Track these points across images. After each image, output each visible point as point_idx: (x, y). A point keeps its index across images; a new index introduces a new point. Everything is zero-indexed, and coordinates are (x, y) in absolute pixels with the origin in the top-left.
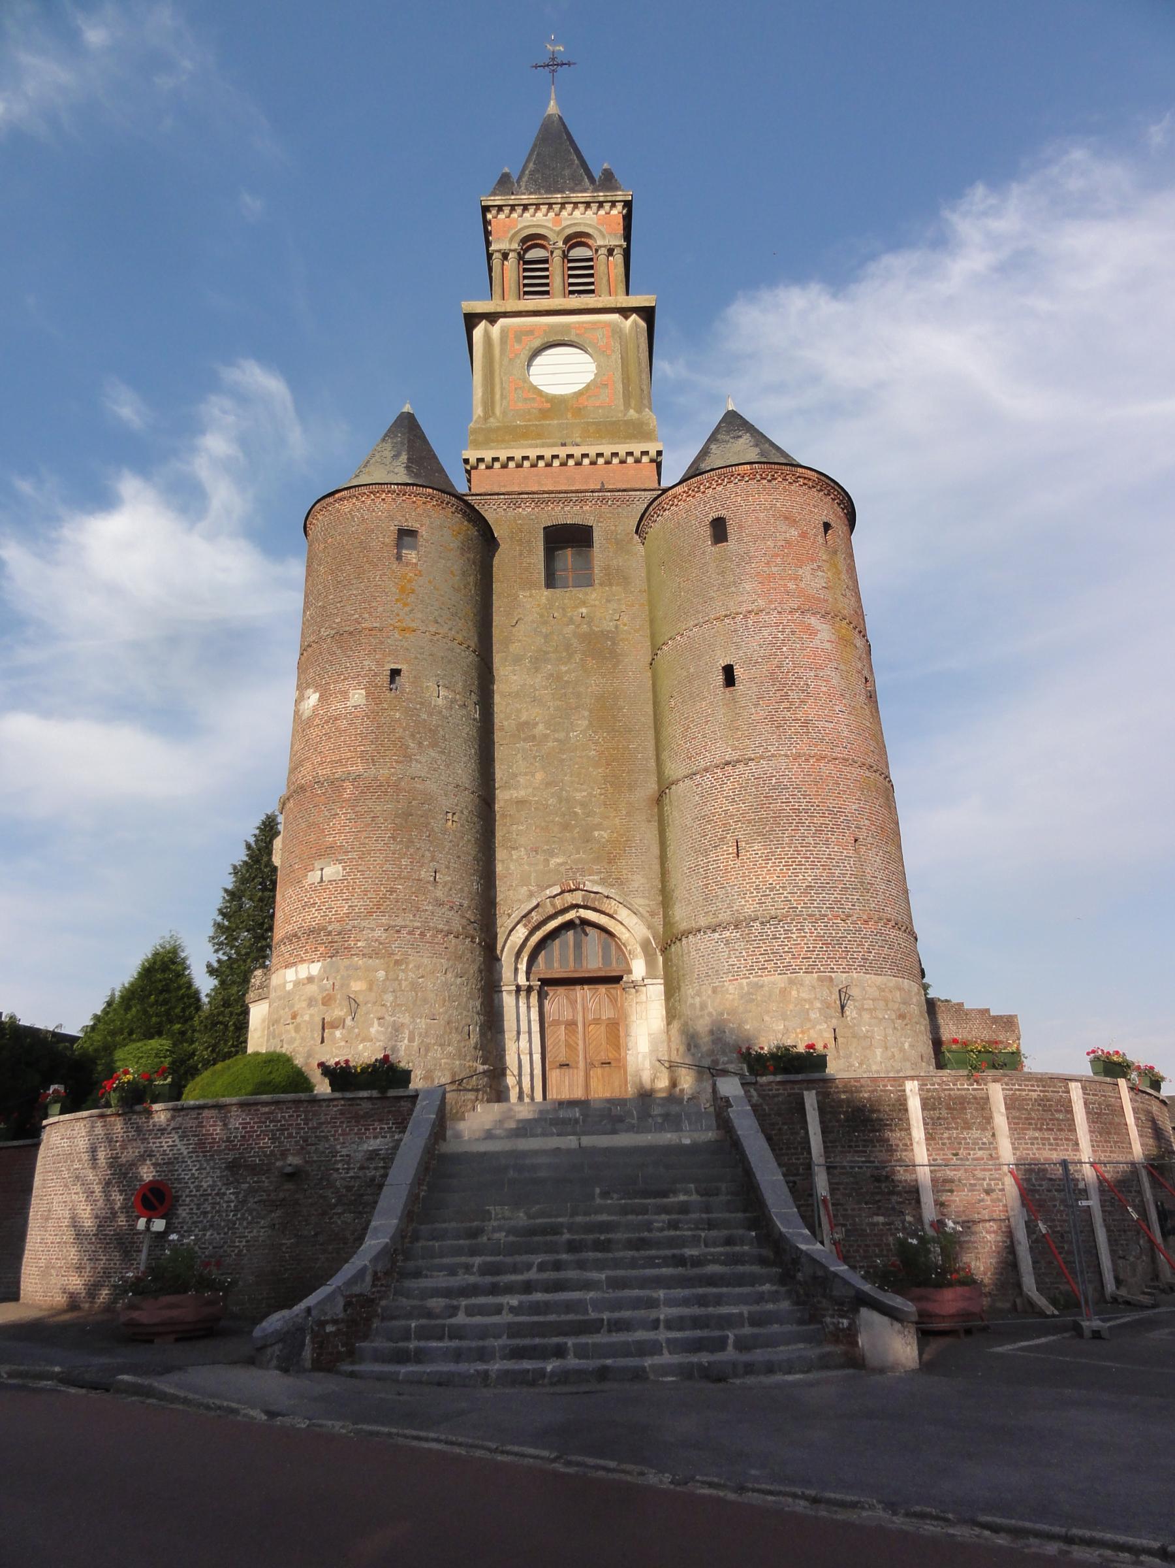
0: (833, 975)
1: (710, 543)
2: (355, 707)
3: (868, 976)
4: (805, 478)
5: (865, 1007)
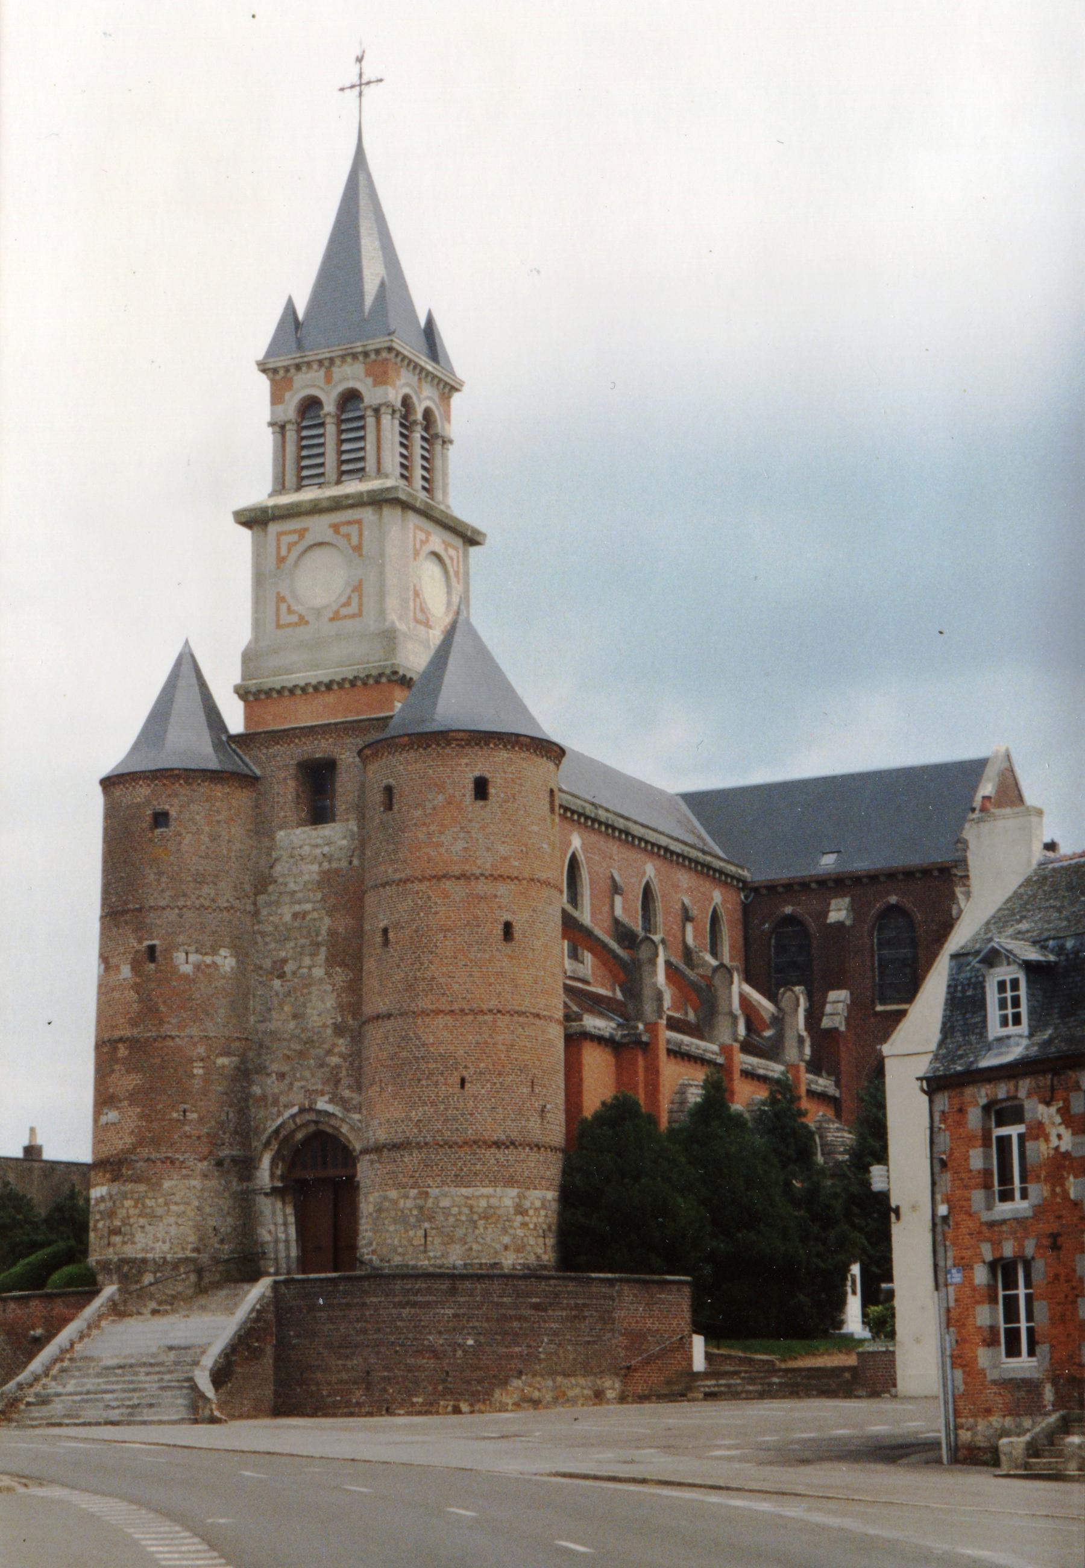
0: (429, 1190)
1: (382, 809)
2: (124, 980)
3: (457, 1189)
4: (457, 740)
5: (453, 1212)
